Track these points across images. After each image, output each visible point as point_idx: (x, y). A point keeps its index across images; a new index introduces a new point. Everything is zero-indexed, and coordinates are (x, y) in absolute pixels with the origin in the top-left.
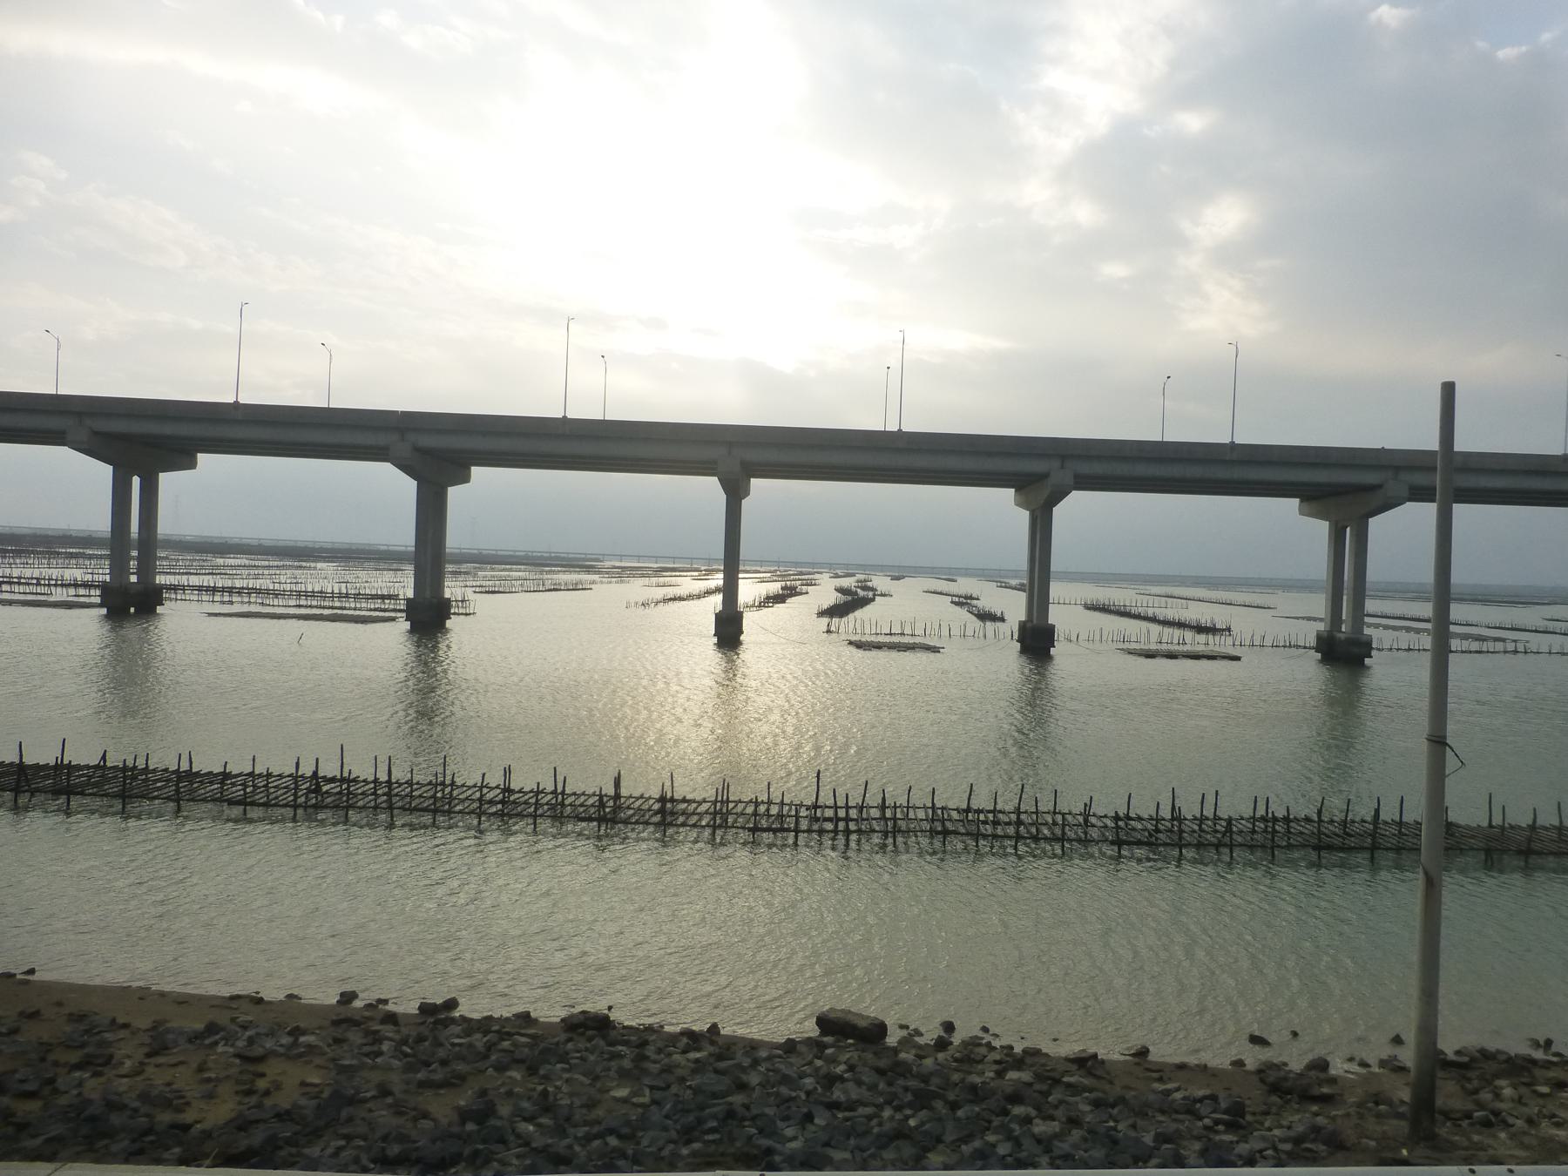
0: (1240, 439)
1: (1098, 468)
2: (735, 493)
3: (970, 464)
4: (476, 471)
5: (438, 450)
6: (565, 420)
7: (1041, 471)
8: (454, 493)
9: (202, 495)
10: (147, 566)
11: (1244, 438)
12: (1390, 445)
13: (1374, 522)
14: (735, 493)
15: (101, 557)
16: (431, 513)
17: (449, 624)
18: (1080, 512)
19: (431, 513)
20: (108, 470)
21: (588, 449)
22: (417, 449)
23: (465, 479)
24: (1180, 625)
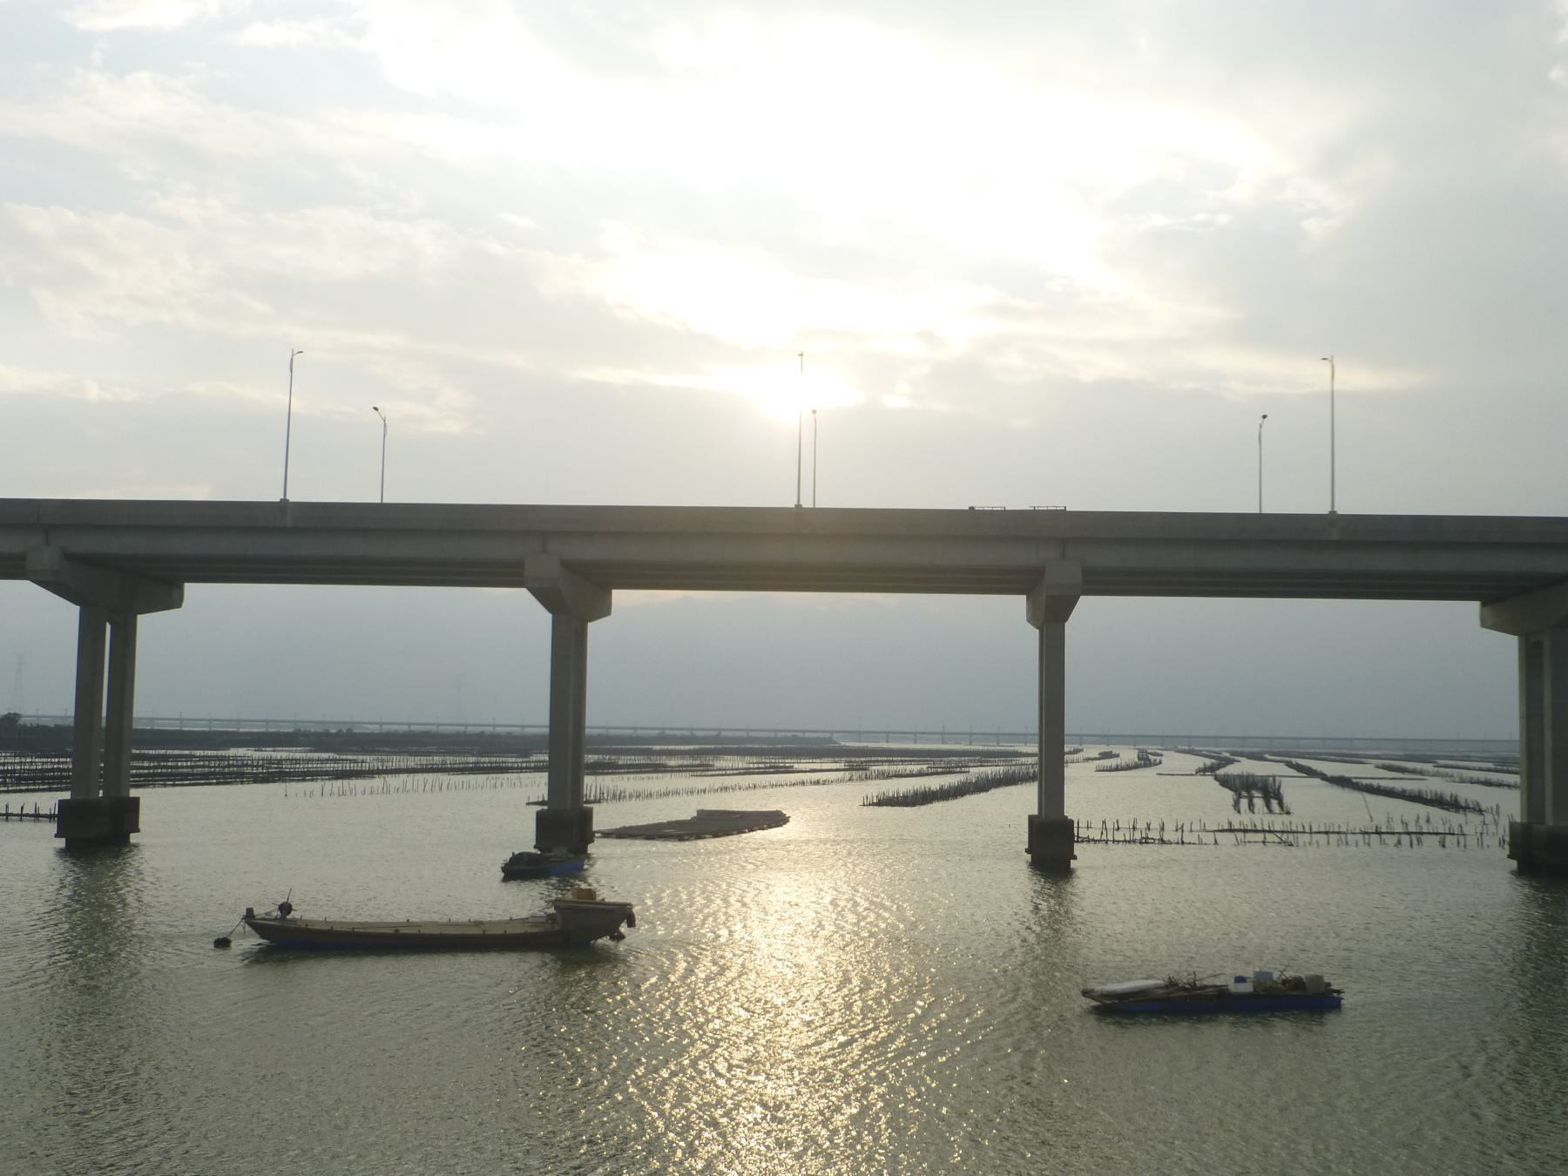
0: (1343, 509)
1: (1106, 558)
2: (1051, 619)
3: (1260, 560)
4: (191, 590)
5: (573, 559)
6: (1332, 519)
7: (1053, 560)
8: (148, 625)
9: (207, 649)
10: (117, 777)
11: (1349, 505)
12: (1011, 506)
13: (77, 609)
14: (1051, 619)
15: (1515, 787)
16: (106, 662)
17: (591, 849)
18: (1096, 619)
19: (106, 662)
20: (73, 611)
21: (258, 547)
22: (68, 557)
23: (174, 601)
24: (1417, 798)
